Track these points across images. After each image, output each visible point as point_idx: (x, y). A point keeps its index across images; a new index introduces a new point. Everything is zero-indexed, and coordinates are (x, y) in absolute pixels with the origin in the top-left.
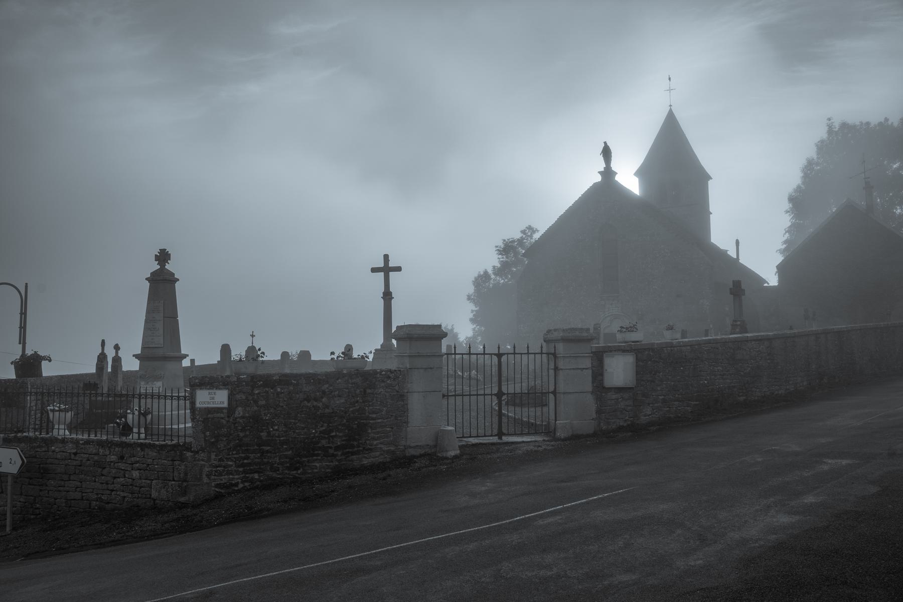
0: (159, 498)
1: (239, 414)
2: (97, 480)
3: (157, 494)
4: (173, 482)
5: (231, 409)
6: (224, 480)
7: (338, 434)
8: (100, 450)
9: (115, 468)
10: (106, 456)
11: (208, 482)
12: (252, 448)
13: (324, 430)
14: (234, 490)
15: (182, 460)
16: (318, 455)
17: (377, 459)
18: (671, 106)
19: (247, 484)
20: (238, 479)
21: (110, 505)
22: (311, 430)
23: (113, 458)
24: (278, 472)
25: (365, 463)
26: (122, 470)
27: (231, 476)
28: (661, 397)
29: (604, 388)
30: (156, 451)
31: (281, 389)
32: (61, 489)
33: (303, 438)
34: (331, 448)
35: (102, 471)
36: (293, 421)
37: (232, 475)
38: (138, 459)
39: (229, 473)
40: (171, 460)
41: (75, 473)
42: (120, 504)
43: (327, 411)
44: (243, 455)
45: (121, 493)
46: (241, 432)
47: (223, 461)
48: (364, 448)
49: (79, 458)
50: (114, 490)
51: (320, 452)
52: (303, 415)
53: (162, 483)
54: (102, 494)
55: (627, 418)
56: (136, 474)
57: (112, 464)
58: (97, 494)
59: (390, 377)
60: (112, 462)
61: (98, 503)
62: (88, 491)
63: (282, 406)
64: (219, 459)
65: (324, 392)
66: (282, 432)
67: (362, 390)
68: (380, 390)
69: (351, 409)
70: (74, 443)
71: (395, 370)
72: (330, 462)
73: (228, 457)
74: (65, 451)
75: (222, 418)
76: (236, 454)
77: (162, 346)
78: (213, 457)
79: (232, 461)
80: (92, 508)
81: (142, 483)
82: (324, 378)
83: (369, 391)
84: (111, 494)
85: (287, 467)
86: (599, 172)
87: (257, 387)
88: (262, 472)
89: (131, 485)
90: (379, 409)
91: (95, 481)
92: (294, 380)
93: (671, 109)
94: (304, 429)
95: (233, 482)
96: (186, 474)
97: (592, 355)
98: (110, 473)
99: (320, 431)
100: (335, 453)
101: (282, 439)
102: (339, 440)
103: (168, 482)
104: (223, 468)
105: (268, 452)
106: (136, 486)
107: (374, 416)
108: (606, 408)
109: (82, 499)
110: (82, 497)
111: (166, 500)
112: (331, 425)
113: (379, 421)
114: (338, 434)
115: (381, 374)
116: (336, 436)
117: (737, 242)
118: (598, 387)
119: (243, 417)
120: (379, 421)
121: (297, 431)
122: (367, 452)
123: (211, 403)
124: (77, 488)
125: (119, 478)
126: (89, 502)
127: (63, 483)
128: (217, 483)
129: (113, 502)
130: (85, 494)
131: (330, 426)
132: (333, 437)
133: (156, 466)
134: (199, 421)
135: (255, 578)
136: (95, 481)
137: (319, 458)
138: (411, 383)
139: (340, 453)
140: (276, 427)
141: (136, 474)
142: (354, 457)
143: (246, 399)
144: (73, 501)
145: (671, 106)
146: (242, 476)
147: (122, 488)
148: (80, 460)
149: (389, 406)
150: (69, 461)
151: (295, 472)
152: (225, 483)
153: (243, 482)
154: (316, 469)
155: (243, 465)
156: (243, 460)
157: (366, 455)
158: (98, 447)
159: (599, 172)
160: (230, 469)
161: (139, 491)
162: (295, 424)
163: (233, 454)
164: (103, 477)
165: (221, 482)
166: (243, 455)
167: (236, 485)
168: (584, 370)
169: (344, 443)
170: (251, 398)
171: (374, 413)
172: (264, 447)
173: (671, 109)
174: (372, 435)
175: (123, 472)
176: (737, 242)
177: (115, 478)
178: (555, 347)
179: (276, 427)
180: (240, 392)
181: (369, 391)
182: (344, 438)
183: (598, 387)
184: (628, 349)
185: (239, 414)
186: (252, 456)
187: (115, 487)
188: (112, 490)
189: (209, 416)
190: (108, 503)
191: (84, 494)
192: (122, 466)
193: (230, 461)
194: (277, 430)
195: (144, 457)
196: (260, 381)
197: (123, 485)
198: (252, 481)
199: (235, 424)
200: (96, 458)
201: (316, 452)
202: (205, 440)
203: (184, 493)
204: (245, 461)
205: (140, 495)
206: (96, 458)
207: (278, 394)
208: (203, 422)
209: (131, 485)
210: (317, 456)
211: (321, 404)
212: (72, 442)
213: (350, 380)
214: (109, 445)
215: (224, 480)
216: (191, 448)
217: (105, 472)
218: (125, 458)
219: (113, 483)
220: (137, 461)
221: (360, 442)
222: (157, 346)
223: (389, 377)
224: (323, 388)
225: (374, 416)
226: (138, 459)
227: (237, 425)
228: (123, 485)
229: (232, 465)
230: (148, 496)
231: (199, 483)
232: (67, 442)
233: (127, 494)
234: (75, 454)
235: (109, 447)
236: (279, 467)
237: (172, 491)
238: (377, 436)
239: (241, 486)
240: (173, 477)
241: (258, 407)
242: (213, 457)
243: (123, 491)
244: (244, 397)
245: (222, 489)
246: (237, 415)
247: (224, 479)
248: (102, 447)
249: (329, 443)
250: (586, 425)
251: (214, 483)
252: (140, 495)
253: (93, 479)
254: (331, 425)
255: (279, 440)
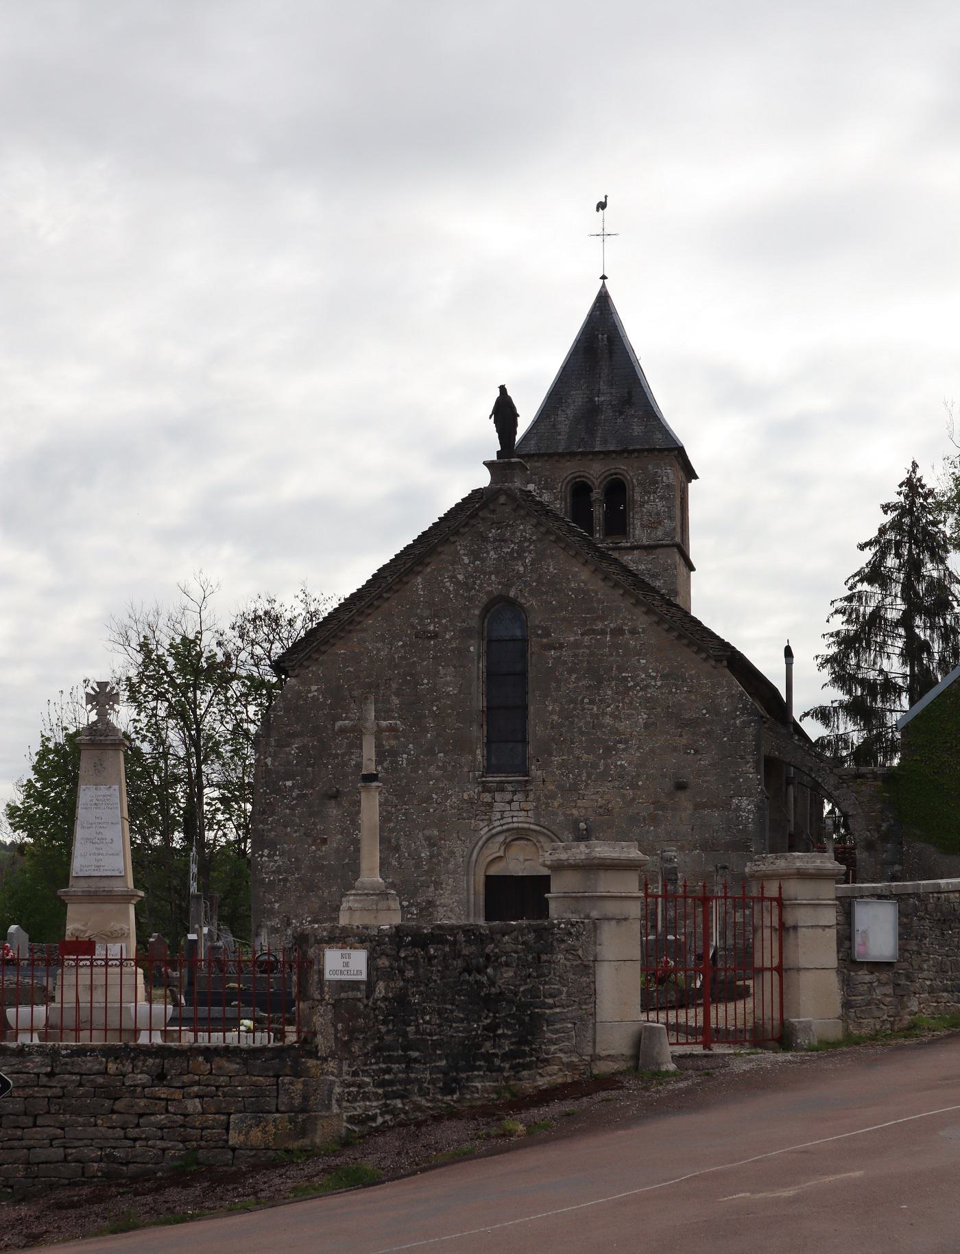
0: (246, 1145)
1: (380, 993)
2: (99, 1122)
3: (242, 1138)
4: (277, 1115)
5: (370, 985)
6: (358, 1109)
7: (506, 1031)
8: (110, 1065)
9: (145, 1097)
10: (124, 1076)
11: (338, 1111)
12: (396, 1054)
13: (488, 1024)
14: (372, 1127)
15: (297, 1075)
16: (479, 1068)
17: (554, 1077)
18: (604, 277)
19: (388, 1117)
20: (376, 1107)
21: (131, 1166)
22: (472, 1023)
23: (142, 1078)
24: (428, 1097)
25: (540, 1083)
26: (160, 1099)
27: (368, 1103)
28: (928, 983)
29: (854, 962)
30: (238, 1060)
31: (435, 950)
32: (15, 1143)
33: (462, 1037)
34: (496, 1055)
35: (114, 1104)
36: (449, 1007)
37: (370, 1100)
38: (197, 1078)
39: (366, 1097)
40: (274, 1076)
41: (48, 1112)
42: (155, 1164)
43: (493, 990)
44: (383, 1066)
45: (158, 1142)
46: (382, 1024)
47: (358, 1075)
48: (538, 1058)
49: (59, 1082)
50: (140, 1139)
51: (482, 1063)
52: (462, 998)
53: (253, 1118)
54: (114, 1148)
55: (885, 1017)
56: (194, 1105)
57: (139, 1089)
58: (101, 1149)
59: (571, 933)
60: (136, 1086)
61: (103, 1165)
62: (80, 1143)
63: (436, 981)
64: (353, 1072)
65: (488, 957)
66: (435, 1027)
67: (534, 955)
68: (559, 957)
69: (522, 989)
70: (48, 1054)
71: (577, 922)
72: (494, 1082)
73: (365, 1068)
74: (24, 1070)
75: (359, 1000)
76: (376, 1063)
77: (123, 874)
78: (345, 1068)
79: (370, 1076)
80: (86, 1175)
81: (206, 1121)
82: (487, 932)
83: (544, 957)
84: (134, 1147)
85: (440, 1088)
86: (486, 463)
87: (404, 946)
88: (407, 1097)
89: (181, 1126)
90: (558, 989)
91: (96, 1125)
92: (450, 935)
93: (604, 284)
94: (463, 1022)
95: (370, 1113)
96: (305, 1098)
97: (837, 902)
98: (133, 1106)
99: (483, 1026)
100: (502, 1065)
101: (435, 1038)
102: (507, 1042)
103: (265, 1115)
104: (356, 1089)
105: (416, 1061)
106: (193, 1128)
107: (550, 1001)
108: (856, 998)
109: (65, 1160)
110: (66, 1156)
111: (263, 1147)
112: (497, 1015)
113: (558, 1010)
114: (506, 1031)
115: (559, 928)
116: (503, 1036)
117: (788, 653)
118: (845, 960)
119: (385, 999)
120: (558, 1010)
121: (454, 1025)
122: (542, 1065)
123: (345, 973)
124: (51, 1140)
125: (152, 1114)
126: (81, 1165)
127: (19, 1132)
128: (349, 1114)
129: (138, 1160)
130: (74, 1151)
131: (497, 1018)
132: (500, 1036)
133: (239, 1088)
134: (328, 1004)
135: (722, 1167)
136: (96, 1125)
137: (481, 1073)
138: (600, 944)
139: (508, 1066)
140: (428, 1018)
141: (194, 1105)
142: (525, 1073)
143: (389, 967)
144: (44, 1166)
145: (604, 277)
146: (381, 1103)
147: (159, 1133)
148: (61, 1087)
149: (571, 984)
150: (36, 1089)
151: (449, 1098)
152: (360, 1115)
153: (382, 1115)
154: (478, 1093)
155: (382, 1084)
156: (384, 1075)
157: (540, 1071)
158: (104, 1059)
159: (486, 463)
160: (366, 1090)
161: (202, 1136)
162: (452, 1011)
163: (371, 1064)
164: (114, 1117)
165: (355, 1113)
166: (383, 1066)
167: (374, 1118)
168: (827, 930)
169: (512, 1047)
170: (396, 965)
171: (552, 996)
172: (411, 1053)
173: (604, 284)
174: (549, 1035)
175: (163, 1103)
176: (788, 653)
177: (141, 1115)
178: (780, 888)
179: (428, 1018)
180: (382, 954)
181: (544, 957)
182: (513, 1040)
183: (845, 960)
184: (888, 893)
185: (380, 993)
186: (395, 1067)
187: (143, 1132)
188: (135, 1140)
189: (343, 995)
190: (127, 1163)
191: (70, 1151)
192: (162, 1092)
193: (367, 1077)
194: (428, 1022)
195: (210, 1073)
196: (407, 935)
197: (161, 1129)
198: (393, 1112)
199: (374, 1010)
200: (100, 1080)
201: (478, 1063)
202: (336, 1038)
203: (303, 1132)
204: (387, 1077)
205: (203, 1143)
206: (100, 1080)
207: (431, 958)
208: (334, 1006)
209: (181, 1126)
210: (479, 1070)
211: (486, 978)
212: (41, 1054)
213: (520, 938)
214: (132, 1055)
215: (358, 1109)
216: (317, 1052)
217: (119, 1105)
218: (169, 1077)
219: (138, 1126)
220: (196, 1081)
221: (534, 1046)
222: (109, 874)
223: (570, 934)
224: (487, 950)
225: (550, 1001)
226: (197, 1078)
227: (377, 1012)
228: (161, 1129)
229: (368, 1084)
230: (221, 1144)
231: (327, 1114)
232: (30, 1054)
233: (173, 1143)
234: (50, 1075)
235: (133, 1059)
236: (429, 1089)
237: (274, 1130)
238: (555, 1036)
239: (380, 1120)
240: (277, 1104)
241: (404, 980)
242: (345, 1068)
243: (162, 1139)
244: (387, 964)
245: (356, 1124)
246: (377, 995)
247: (359, 1108)
248: (116, 1058)
249: (494, 1048)
250: (835, 1032)
251: (346, 1114)
252: (203, 1143)
253: (92, 1120)
254: (497, 1015)
255: (432, 1040)
